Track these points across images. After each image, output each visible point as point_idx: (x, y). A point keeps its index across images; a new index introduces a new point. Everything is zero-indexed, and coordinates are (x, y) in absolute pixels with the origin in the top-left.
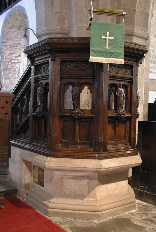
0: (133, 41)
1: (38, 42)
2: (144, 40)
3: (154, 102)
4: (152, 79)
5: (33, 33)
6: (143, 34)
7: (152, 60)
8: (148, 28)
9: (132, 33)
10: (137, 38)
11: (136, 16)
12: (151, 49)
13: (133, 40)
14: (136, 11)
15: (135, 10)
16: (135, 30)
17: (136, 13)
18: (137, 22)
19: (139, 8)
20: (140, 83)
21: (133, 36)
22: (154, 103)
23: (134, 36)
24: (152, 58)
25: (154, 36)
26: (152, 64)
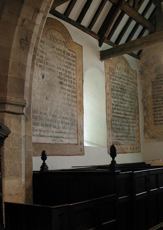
0: (6, 109)
1: (84, 145)
2: (21, 108)
3: (40, 168)
4: (46, 143)
5: (80, 166)
6: (19, 101)
7: (45, 124)
8: (24, 95)
9: (4, 101)
10: (11, 106)
11: (8, 83)
12: (43, 112)
13: (6, 108)
14: (9, 77)
15: (8, 76)
16: (8, 97)
17: (9, 79)
18: (11, 88)
19: (13, 74)
20: (17, 155)
21: (6, 105)
22: (41, 169)
23: (7, 104)
24: (44, 121)
25: (45, 98)
26: (45, 127)
